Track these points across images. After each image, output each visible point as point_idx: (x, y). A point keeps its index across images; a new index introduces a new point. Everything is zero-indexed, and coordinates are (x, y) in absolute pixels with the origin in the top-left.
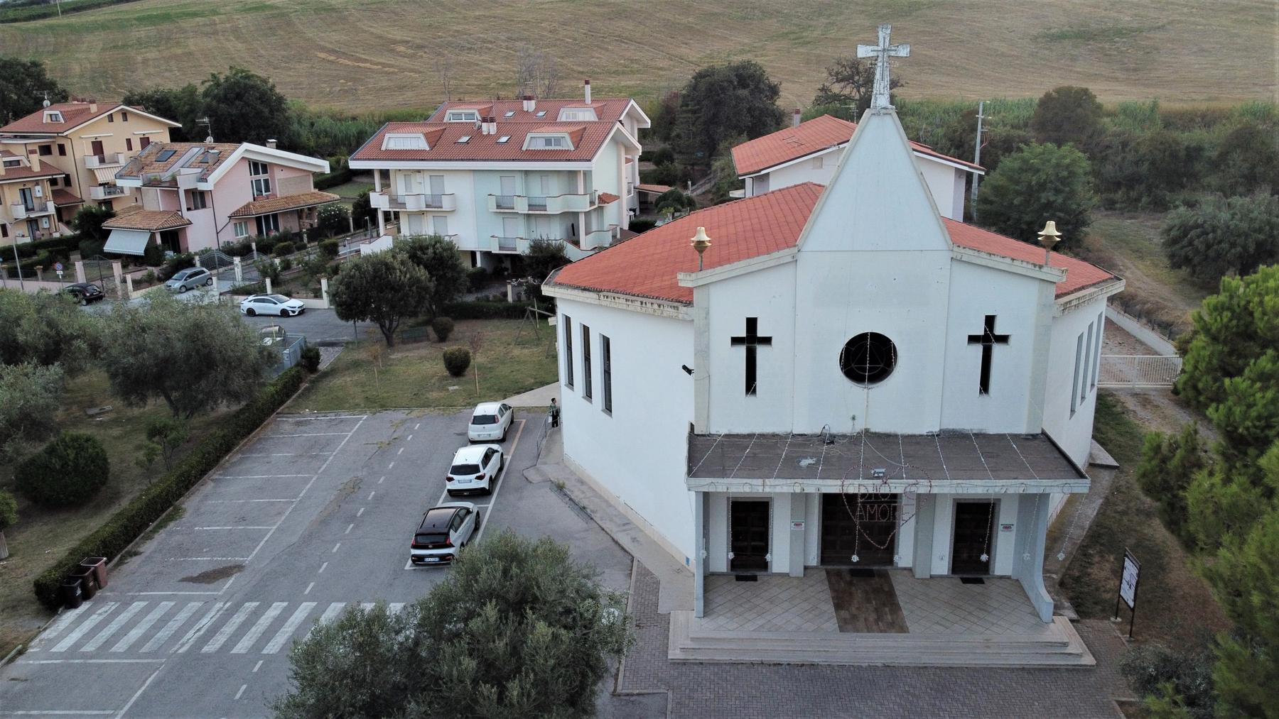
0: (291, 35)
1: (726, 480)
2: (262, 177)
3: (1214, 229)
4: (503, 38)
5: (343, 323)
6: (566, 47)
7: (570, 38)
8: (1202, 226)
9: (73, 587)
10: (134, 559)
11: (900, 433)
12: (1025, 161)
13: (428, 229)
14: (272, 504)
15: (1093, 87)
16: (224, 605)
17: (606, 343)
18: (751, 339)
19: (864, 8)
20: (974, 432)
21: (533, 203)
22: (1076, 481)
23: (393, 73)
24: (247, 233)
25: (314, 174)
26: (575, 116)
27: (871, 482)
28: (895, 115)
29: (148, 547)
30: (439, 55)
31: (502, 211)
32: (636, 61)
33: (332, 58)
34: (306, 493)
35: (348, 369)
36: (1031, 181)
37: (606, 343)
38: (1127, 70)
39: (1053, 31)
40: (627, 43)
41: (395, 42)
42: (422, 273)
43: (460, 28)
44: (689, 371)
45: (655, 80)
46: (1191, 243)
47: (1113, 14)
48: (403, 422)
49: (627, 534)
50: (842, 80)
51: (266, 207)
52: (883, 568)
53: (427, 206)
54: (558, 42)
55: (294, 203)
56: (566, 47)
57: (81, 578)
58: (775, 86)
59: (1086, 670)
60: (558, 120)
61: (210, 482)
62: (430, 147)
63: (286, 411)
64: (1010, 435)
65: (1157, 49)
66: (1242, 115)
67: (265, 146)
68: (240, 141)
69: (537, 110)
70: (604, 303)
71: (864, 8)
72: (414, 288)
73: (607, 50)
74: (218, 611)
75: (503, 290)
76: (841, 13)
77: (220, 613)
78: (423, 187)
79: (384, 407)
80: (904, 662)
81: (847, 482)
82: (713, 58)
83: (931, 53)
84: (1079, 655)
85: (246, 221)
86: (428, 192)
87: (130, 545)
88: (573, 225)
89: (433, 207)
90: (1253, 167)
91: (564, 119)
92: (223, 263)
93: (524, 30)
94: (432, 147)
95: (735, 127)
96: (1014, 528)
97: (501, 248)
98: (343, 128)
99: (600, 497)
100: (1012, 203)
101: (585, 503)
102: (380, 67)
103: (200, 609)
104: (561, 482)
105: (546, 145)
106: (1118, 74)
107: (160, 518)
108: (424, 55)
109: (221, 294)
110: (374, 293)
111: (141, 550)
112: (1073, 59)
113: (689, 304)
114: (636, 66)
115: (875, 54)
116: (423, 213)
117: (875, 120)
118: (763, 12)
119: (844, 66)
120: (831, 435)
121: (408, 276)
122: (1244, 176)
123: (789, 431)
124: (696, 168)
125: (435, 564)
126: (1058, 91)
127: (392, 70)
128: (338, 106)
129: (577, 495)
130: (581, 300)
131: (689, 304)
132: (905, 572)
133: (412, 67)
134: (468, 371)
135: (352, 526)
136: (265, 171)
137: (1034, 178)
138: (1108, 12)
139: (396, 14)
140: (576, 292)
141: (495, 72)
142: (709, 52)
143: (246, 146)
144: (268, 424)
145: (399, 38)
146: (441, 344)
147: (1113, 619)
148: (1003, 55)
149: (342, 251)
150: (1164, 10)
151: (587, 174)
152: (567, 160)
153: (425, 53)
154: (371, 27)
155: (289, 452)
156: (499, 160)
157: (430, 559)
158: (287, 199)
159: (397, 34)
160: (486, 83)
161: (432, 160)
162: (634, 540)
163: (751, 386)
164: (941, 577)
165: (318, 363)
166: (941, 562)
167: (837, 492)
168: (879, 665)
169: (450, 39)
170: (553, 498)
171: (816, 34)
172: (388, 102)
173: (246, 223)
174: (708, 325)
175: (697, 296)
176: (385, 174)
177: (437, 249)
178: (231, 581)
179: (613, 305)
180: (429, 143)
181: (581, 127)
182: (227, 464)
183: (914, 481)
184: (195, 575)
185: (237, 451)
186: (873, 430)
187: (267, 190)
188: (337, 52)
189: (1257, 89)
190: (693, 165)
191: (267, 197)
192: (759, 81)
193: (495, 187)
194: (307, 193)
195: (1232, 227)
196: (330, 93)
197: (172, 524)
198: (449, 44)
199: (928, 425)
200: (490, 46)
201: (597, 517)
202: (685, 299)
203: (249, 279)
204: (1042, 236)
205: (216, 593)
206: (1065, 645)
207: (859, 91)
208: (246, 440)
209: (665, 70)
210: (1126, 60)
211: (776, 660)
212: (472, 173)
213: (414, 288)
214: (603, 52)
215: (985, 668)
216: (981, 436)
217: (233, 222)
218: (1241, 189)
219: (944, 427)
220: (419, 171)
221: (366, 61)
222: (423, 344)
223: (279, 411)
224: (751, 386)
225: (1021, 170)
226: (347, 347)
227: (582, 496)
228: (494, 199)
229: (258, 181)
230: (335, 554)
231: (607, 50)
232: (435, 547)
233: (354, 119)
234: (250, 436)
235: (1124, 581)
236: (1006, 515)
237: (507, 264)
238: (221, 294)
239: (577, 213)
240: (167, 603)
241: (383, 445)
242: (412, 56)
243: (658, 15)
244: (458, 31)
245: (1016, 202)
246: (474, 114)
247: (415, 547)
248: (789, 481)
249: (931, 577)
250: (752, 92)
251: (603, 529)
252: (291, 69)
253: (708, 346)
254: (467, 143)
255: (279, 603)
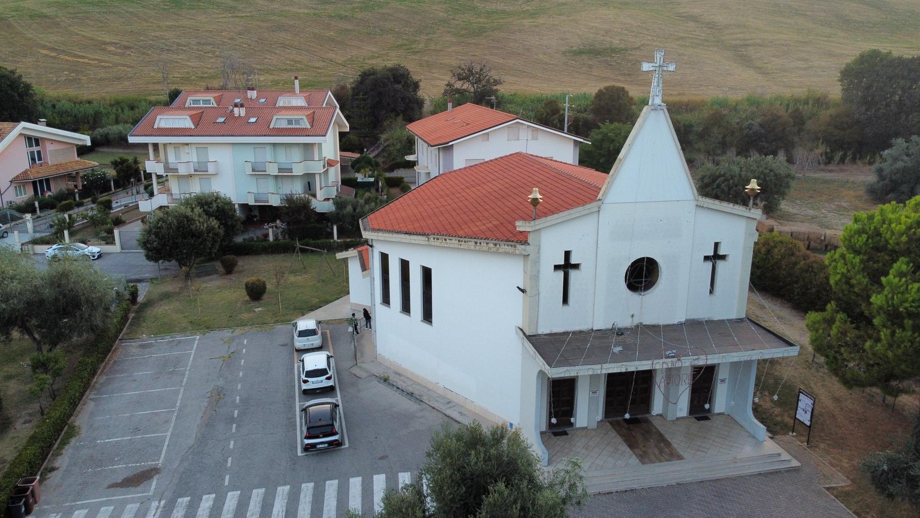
0: (13, 35)
1: (577, 368)
2: (35, 149)
3: (732, 177)
4: (194, 43)
5: (147, 262)
6: (244, 50)
7: (246, 44)
8: (723, 175)
9: (20, 506)
10: (55, 473)
11: (661, 324)
12: (605, 135)
13: (196, 188)
14: (156, 414)
15: (627, 87)
16: (159, 503)
17: (427, 274)
18: (567, 266)
19: (449, 29)
20: (706, 319)
21: (283, 166)
22: (787, 348)
23: (108, 67)
24: (25, 194)
25: (77, 145)
26: (290, 102)
27: (670, 360)
28: (666, 110)
29: (62, 462)
30: (143, 54)
31: (257, 173)
32: (299, 62)
33: (53, 54)
34: (181, 403)
35: (162, 300)
36: (609, 148)
37: (427, 274)
38: (624, 75)
39: (574, 48)
40: (289, 49)
41: (105, 43)
42: (214, 223)
43: (157, 34)
44: (523, 291)
45: (317, 77)
46: (718, 186)
47: (608, 39)
48: (232, 339)
49: (455, 410)
50: (462, 79)
51: (40, 173)
52: (644, 416)
53: (195, 171)
54: (237, 47)
55: (64, 169)
56: (244, 50)
57: (24, 497)
58: (417, 82)
59: (795, 470)
60: (277, 106)
61: (89, 401)
62: (195, 126)
63: (126, 337)
64: (727, 320)
65: (638, 62)
66: (712, 105)
67: (37, 124)
68: (17, 120)
69: (258, 98)
70: (433, 244)
71: (449, 29)
72: (211, 235)
73: (276, 53)
74: (157, 509)
75: (265, 232)
76: (435, 33)
77: (159, 510)
78: (192, 156)
79: (209, 328)
80: (689, 480)
81: (655, 362)
82: (353, 61)
83: (501, 61)
84: (789, 461)
85: (24, 184)
86: (195, 160)
87: (45, 463)
88: (309, 183)
89: (201, 171)
90: (724, 137)
91: (281, 105)
92: (14, 219)
93: (210, 37)
94: (197, 125)
95: (394, 110)
96: (727, 380)
97: (256, 201)
98: (82, 109)
99: (419, 384)
100: (599, 162)
101: (411, 389)
102: (96, 62)
103: (138, 510)
104: (386, 376)
105: (288, 124)
106: (620, 78)
107: (60, 437)
108: (132, 54)
109: (22, 245)
110: (180, 240)
111: (56, 465)
112: (590, 67)
113: (525, 243)
114: (299, 66)
115: (654, 69)
116: (191, 176)
117: (653, 114)
118: (381, 30)
119: (463, 69)
120: (620, 329)
121: (205, 225)
122: (719, 143)
123: (590, 328)
124: (367, 139)
125: (325, 449)
126: (607, 88)
127: (107, 65)
128: (72, 92)
129: (400, 384)
130: (407, 241)
131: (525, 243)
132: (658, 417)
133: (124, 63)
134: (265, 296)
135: (234, 426)
136: (37, 144)
137: (611, 145)
138: (604, 37)
139: (101, 22)
140: (403, 236)
141: (193, 68)
142: (349, 57)
143: (23, 124)
144: (116, 349)
145: (108, 40)
146: (229, 276)
147: (791, 434)
148: (546, 63)
149: (114, 205)
150: (637, 37)
151: (320, 145)
152: (307, 136)
153: (132, 52)
154: (82, 31)
155: (147, 371)
156: (253, 136)
157: (321, 446)
158: (58, 166)
159: (107, 38)
160: (188, 76)
161: (199, 136)
162: (460, 413)
163: (565, 300)
164: (683, 418)
165: (137, 296)
166: (683, 407)
167: (649, 369)
168: (674, 484)
169: (151, 42)
170: (383, 388)
171: (421, 46)
172: (110, 89)
173: (24, 186)
174: (539, 258)
175: (531, 239)
176: (156, 146)
177: (219, 203)
178: (154, 482)
179: (443, 245)
180: (194, 123)
181: (311, 111)
182: (97, 386)
183: (697, 357)
184: (120, 481)
185: (100, 374)
186: (644, 323)
187: (40, 159)
188: (56, 50)
189: (703, 88)
190: (365, 137)
191: (41, 165)
192: (407, 79)
193: (250, 155)
194: (72, 162)
195: (743, 176)
196: (57, 81)
197: (73, 441)
198: (151, 46)
199: (679, 317)
200: (184, 48)
201: (425, 399)
202: (522, 239)
203: (39, 232)
204: (747, 189)
205: (146, 494)
206: (779, 455)
207: (474, 87)
208: (104, 364)
209: (321, 69)
210: (622, 69)
211: (608, 490)
212: (231, 146)
213: (211, 235)
214: (273, 55)
215: (738, 477)
216: (710, 322)
217: (14, 185)
218: (719, 152)
219: (688, 318)
220: (187, 144)
221: (83, 57)
222: (214, 276)
223: (120, 337)
224: (565, 300)
225: (602, 140)
226: (153, 282)
227: (405, 385)
228: (250, 165)
229: (32, 153)
230: (234, 448)
231: (276, 53)
232: (325, 436)
233: (89, 102)
234: (106, 360)
235: (799, 409)
236: (722, 374)
237: (256, 213)
238: (22, 245)
239: (314, 174)
240: (106, 508)
241: (226, 359)
242: (122, 55)
243: (308, 30)
244: (157, 37)
245: (601, 161)
246: (210, 100)
247: (307, 437)
248: (618, 364)
249: (678, 419)
250: (403, 86)
251: (434, 408)
252: (19, 62)
253: (538, 272)
254: (224, 122)
255: (207, 496)
